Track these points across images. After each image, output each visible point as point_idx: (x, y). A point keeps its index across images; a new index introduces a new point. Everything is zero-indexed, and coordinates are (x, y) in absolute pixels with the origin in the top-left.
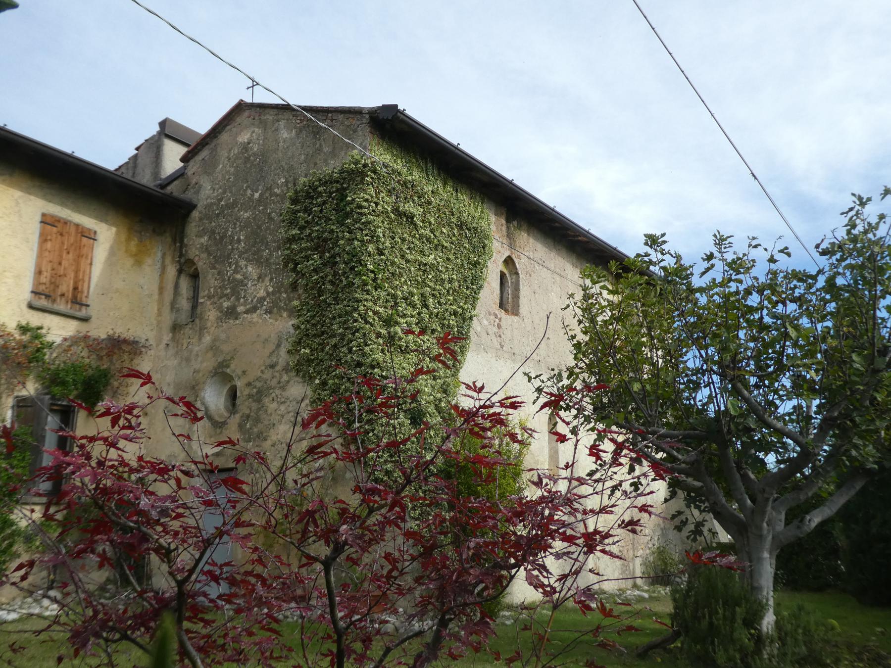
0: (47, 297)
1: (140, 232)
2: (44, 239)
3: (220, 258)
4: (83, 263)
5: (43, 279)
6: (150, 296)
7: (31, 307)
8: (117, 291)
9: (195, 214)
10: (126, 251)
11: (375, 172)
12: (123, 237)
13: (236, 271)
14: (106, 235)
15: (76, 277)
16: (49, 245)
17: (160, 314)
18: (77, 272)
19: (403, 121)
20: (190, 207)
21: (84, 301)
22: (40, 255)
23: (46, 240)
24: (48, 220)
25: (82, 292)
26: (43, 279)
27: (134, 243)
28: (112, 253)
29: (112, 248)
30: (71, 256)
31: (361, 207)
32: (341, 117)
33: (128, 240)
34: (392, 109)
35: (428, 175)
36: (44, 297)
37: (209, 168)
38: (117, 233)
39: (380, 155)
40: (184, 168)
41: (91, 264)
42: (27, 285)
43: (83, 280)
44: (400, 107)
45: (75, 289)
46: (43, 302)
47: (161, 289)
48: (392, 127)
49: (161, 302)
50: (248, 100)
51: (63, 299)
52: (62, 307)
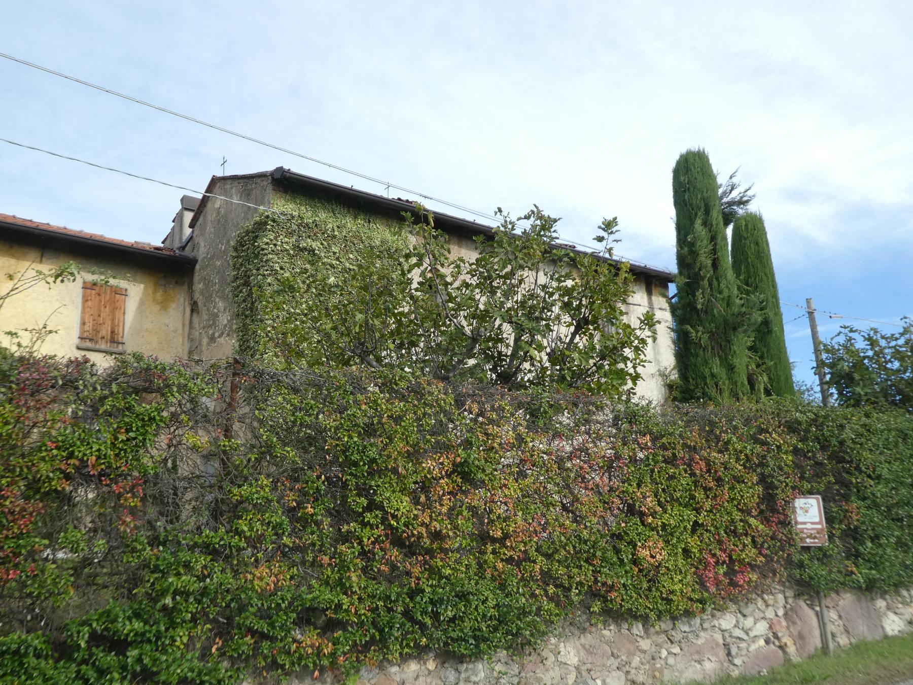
0: (91, 340)
1: (165, 285)
2: (85, 300)
3: (208, 299)
4: (118, 314)
5: (87, 328)
6: (175, 331)
7: (78, 348)
8: (147, 330)
9: (198, 267)
10: (154, 301)
11: (274, 221)
12: (150, 291)
13: (214, 307)
14: (135, 291)
15: (113, 323)
16: (90, 303)
17: (183, 345)
18: (113, 320)
19: (290, 178)
20: (193, 262)
21: (120, 340)
22: (83, 312)
23: (87, 300)
24: (89, 286)
25: (118, 334)
26: (87, 328)
27: (159, 294)
28: (142, 303)
29: (141, 299)
30: (107, 309)
31: (263, 249)
32: (259, 180)
33: (155, 292)
34: (280, 169)
35: (334, 214)
36: (89, 339)
37: (203, 228)
38: (145, 288)
39: (281, 206)
40: (193, 232)
41: (124, 313)
42: (75, 333)
43: (118, 325)
44: (286, 167)
45: (113, 332)
46: (89, 344)
47: (183, 325)
48: (287, 183)
49: (184, 337)
50: (220, 174)
51: (104, 341)
52: (103, 346)
